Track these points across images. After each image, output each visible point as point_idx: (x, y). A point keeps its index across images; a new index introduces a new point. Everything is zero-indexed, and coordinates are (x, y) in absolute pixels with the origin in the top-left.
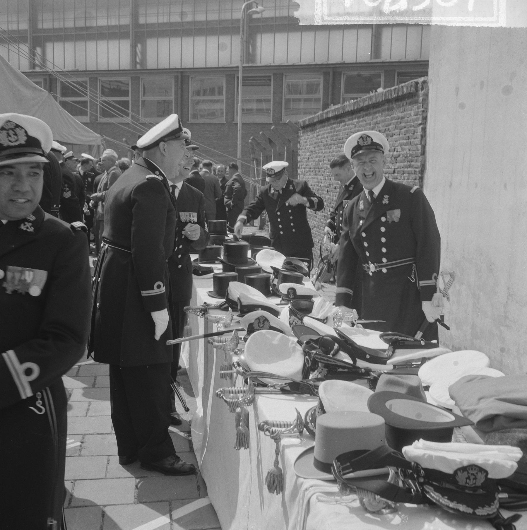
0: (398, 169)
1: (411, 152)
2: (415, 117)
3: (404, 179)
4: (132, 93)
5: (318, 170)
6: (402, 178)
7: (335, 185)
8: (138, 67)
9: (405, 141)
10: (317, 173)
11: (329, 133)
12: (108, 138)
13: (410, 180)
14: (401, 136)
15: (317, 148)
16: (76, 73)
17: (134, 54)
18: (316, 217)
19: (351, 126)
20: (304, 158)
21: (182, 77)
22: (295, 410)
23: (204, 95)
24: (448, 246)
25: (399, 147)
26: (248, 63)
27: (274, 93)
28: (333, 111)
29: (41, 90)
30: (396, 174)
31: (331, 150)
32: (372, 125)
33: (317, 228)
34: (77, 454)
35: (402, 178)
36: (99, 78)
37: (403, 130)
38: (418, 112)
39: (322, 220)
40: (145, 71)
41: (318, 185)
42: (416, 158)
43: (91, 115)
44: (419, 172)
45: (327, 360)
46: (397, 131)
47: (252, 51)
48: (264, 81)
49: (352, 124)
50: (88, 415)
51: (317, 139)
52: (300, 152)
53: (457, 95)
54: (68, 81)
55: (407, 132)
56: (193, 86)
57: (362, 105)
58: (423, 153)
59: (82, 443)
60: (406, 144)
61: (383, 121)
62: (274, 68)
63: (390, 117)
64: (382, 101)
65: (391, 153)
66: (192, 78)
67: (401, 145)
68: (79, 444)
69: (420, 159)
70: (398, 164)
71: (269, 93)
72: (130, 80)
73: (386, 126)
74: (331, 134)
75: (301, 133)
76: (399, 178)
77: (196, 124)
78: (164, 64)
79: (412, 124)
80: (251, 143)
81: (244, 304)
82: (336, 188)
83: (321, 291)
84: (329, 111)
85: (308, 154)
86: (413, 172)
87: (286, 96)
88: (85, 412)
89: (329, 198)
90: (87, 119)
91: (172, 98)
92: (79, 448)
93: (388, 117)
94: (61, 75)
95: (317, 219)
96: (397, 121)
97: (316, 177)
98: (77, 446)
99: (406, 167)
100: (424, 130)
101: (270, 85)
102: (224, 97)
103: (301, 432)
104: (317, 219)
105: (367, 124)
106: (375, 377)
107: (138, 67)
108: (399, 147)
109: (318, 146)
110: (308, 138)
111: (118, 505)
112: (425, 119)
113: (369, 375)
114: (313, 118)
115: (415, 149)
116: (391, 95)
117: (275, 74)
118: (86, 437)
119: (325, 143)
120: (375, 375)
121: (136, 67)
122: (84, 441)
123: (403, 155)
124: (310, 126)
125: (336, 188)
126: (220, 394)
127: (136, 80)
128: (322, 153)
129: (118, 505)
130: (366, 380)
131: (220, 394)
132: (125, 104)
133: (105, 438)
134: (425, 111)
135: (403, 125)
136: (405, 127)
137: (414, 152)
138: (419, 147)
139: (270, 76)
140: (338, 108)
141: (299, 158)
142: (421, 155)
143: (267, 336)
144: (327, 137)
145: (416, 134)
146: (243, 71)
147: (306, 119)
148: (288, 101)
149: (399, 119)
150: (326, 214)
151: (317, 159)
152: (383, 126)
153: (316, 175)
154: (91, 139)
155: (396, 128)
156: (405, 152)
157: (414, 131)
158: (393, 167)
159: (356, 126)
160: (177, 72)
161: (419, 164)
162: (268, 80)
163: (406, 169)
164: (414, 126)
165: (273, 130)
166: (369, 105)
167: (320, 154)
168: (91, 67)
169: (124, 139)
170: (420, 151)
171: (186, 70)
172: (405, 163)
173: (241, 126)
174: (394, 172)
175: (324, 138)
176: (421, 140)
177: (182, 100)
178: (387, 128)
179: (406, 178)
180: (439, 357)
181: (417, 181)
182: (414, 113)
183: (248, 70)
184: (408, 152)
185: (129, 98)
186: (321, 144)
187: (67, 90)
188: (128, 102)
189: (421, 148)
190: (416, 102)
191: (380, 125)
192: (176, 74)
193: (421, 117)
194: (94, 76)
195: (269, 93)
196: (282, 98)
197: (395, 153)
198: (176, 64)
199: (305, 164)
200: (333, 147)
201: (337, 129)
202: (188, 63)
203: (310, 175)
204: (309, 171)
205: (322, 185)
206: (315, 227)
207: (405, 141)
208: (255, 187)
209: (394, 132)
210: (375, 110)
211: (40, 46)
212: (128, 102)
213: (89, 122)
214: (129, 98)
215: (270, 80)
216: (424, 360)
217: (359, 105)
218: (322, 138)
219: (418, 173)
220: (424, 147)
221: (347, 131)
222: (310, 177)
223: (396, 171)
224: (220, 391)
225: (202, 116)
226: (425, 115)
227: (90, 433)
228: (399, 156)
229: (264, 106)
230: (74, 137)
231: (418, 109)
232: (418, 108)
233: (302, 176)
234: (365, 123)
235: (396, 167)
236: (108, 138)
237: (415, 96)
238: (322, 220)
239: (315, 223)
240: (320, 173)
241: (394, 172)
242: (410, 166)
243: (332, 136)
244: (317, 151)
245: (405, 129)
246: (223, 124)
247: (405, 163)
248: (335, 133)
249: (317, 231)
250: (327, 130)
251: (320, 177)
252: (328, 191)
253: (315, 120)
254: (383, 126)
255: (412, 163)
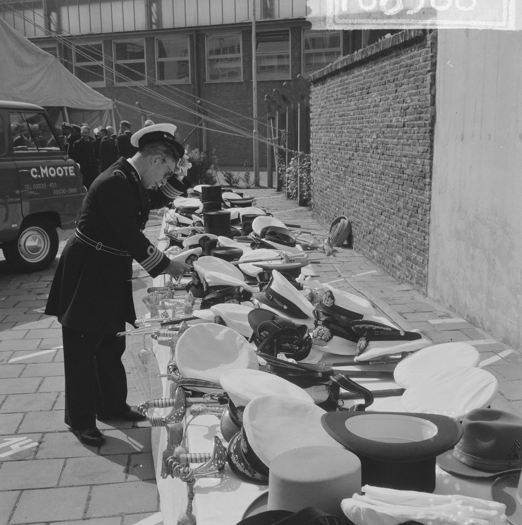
0: (408, 123)
1: (420, 103)
2: (424, 63)
3: (414, 133)
4: (147, 54)
5: (329, 127)
6: (412, 132)
7: (346, 143)
8: (154, 27)
9: (414, 91)
10: (329, 130)
11: (339, 86)
12: (119, 102)
13: (420, 134)
14: (410, 85)
15: (328, 103)
16: (91, 36)
17: (149, 14)
18: (329, 177)
19: (360, 77)
20: (316, 115)
21: (197, 35)
22: (404, 327)
23: (224, 53)
24: (460, 205)
25: (408, 98)
26: (266, 18)
27: (292, 48)
28: (341, 62)
29: (47, 56)
30: (406, 128)
31: (341, 105)
32: (381, 76)
33: (330, 189)
34: (31, 457)
35: (412, 132)
36: (113, 41)
37: (412, 79)
38: (427, 57)
39: (334, 180)
40: (161, 31)
41: (330, 143)
42: (426, 109)
43: (107, 80)
44: (429, 124)
45: (275, 363)
46: (405, 80)
47: (270, 5)
48: (282, 36)
49: (361, 75)
50: (54, 409)
51: (327, 94)
52: (312, 109)
53: (467, 36)
54: (79, 45)
55: (416, 80)
56: (209, 45)
57: (369, 53)
58: (433, 103)
59: (40, 443)
60: (416, 94)
61: (392, 70)
62: (291, 21)
63: (398, 65)
64: (389, 48)
65: (401, 105)
66: (207, 36)
67: (410, 95)
68: (36, 444)
69: (430, 109)
70: (407, 116)
71: (287, 48)
72: (145, 41)
73: (395, 76)
74: (340, 88)
75: (312, 88)
76: (409, 132)
77: (213, 84)
78: (180, 23)
79: (421, 71)
80: (266, 101)
81: (210, 285)
82: (347, 146)
83: (332, 256)
84: (338, 63)
85: (319, 110)
86: (423, 125)
87: (304, 52)
88: (51, 405)
89: (341, 157)
90: (102, 84)
91: (188, 58)
92: (35, 449)
93: (396, 65)
94: (69, 39)
95: (330, 179)
96: (405, 69)
97: (328, 134)
98: (33, 448)
99: (416, 119)
100: (433, 77)
101: (288, 40)
102: (241, 55)
103: (221, 469)
104: (330, 179)
105: (375, 75)
106: (334, 383)
107: (154, 27)
108: (408, 98)
109: (329, 101)
110: (319, 93)
111: (64, 521)
112: (434, 65)
113: (329, 379)
114: (323, 71)
115: (424, 99)
116: (399, 40)
117: (292, 28)
118: (47, 435)
119: (336, 97)
120: (334, 380)
121: (151, 27)
122: (43, 440)
123: (412, 106)
124: (321, 80)
125: (347, 146)
126: (142, 409)
127: (150, 40)
128: (333, 108)
129: (64, 521)
130: (325, 386)
131: (142, 409)
132: (140, 67)
133: (66, 437)
134: (434, 56)
135: (412, 73)
136: (414, 76)
137: (423, 102)
138: (429, 96)
139: (288, 31)
140: (346, 59)
141: (311, 115)
142: (431, 105)
143: (210, 330)
144: (337, 91)
145: (425, 82)
146: (257, 26)
147: (316, 74)
148: (309, 56)
149: (407, 67)
150: (338, 174)
151: (328, 115)
152: (392, 76)
153: (328, 132)
154: (102, 104)
155: (405, 77)
156: (414, 103)
157: (423, 79)
158: (403, 121)
159: (365, 78)
160: (192, 31)
161: (429, 116)
162: (286, 35)
163: (415, 122)
164: (422, 74)
165: (285, 87)
166: (377, 53)
167: (331, 110)
168: (107, 29)
169: (137, 103)
170: (430, 101)
171: (200, 28)
172: (415, 116)
173: (256, 83)
174: (404, 126)
175: (334, 92)
176: (431, 89)
177: (198, 60)
178: (396, 77)
179: (416, 132)
180: (419, 352)
181: (427, 135)
182: (423, 59)
183: (263, 25)
184: (418, 103)
185: (144, 61)
186: (331, 98)
187: (82, 56)
188: (144, 64)
189: (431, 98)
190: (424, 46)
191: (389, 75)
192: (191, 33)
193: (430, 63)
194: (108, 38)
195: (287, 48)
196: (301, 53)
197: (405, 105)
198: (192, 22)
199: (317, 121)
200: (344, 102)
201: (346, 81)
202: (204, 21)
203: (322, 132)
204: (321, 128)
205: (334, 143)
206: (328, 187)
207: (414, 91)
208: (272, 147)
209: (403, 81)
210: (383, 59)
211: (55, 11)
212: (144, 64)
213: (105, 86)
214: (144, 61)
215: (288, 35)
216: (405, 354)
217: (367, 54)
218: (332, 92)
219: (428, 126)
220: (434, 97)
221: (356, 83)
222: (322, 134)
223: (406, 125)
224: (142, 406)
225: (223, 76)
226: (434, 61)
227: (51, 430)
228: (408, 108)
229: (285, 62)
230: (82, 102)
231: (427, 54)
232: (427, 53)
233: (314, 134)
234: (373, 73)
235: (406, 120)
236: (119, 102)
237: (423, 40)
238: (334, 180)
239: (328, 183)
240: (332, 130)
241: (404, 126)
242: (420, 119)
243: (342, 90)
244: (328, 107)
245: (414, 78)
246: (241, 83)
247: (415, 116)
248: (345, 86)
249: (330, 192)
250: (337, 83)
251: (331, 134)
252: (339, 149)
253: (325, 73)
254: (392, 76)
255: (422, 115)
